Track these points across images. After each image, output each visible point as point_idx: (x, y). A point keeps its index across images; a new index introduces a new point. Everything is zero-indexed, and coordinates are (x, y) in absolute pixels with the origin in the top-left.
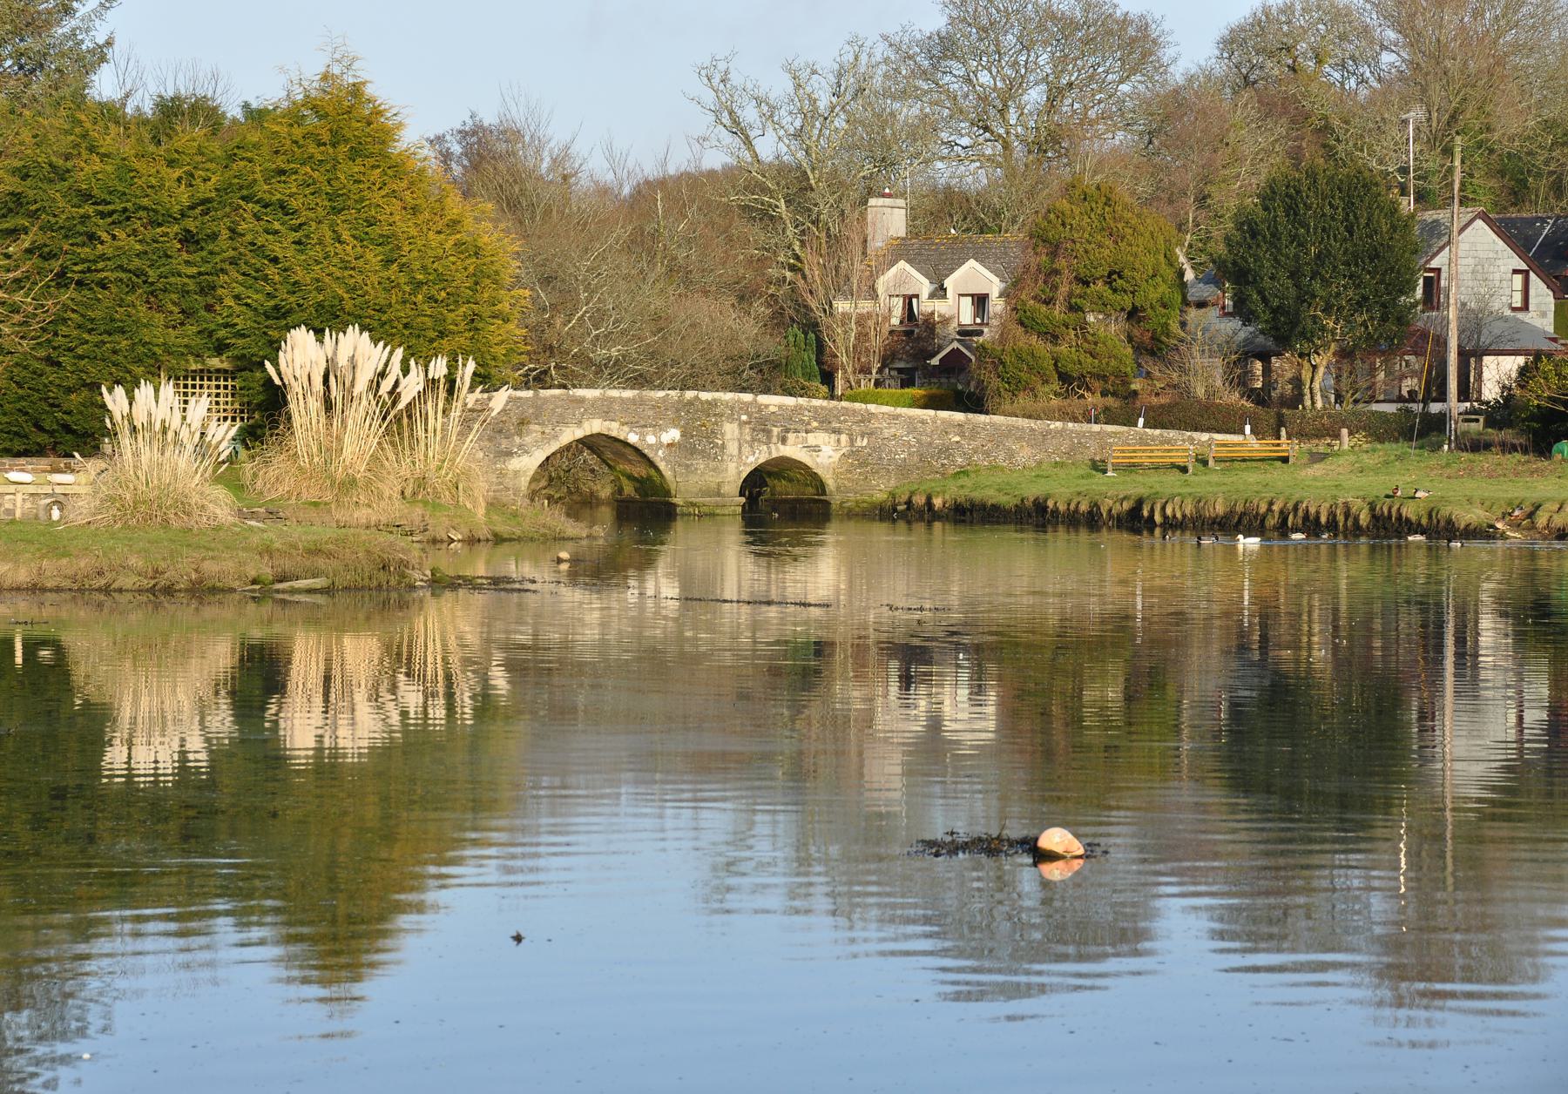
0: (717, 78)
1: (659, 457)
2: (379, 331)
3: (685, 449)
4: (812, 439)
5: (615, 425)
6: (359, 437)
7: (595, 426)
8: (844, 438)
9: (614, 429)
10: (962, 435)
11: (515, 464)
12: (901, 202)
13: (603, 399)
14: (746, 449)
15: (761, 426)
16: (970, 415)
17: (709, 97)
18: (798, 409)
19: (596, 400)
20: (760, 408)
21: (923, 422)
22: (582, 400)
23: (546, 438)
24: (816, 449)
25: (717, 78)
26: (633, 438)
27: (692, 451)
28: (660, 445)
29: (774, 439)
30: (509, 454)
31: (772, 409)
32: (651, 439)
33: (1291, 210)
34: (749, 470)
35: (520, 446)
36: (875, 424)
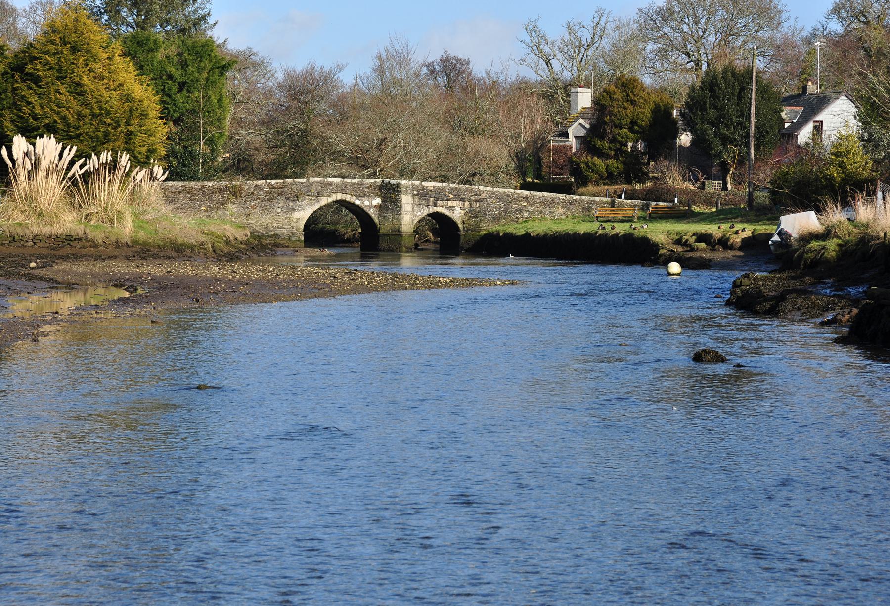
0: (532, 29)
1: (372, 212)
2: (65, 137)
3: (381, 208)
4: (450, 203)
5: (348, 196)
6: (50, 190)
7: (339, 197)
8: (467, 203)
9: (348, 198)
10: (528, 202)
11: (296, 215)
12: (589, 90)
13: (343, 183)
14: (416, 208)
15: (423, 196)
16: (532, 192)
17: (528, 39)
18: (443, 189)
19: (339, 183)
20: (424, 188)
21: (507, 196)
22: (331, 184)
23: (311, 203)
24: (452, 208)
25: (532, 29)
26: (358, 202)
27: (387, 209)
28: (371, 206)
29: (431, 204)
30: (294, 210)
31: (430, 188)
32: (367, 203)
33: (712, 90)
34: (417, 219)
35: (299, 206)
36: (483, 197)
